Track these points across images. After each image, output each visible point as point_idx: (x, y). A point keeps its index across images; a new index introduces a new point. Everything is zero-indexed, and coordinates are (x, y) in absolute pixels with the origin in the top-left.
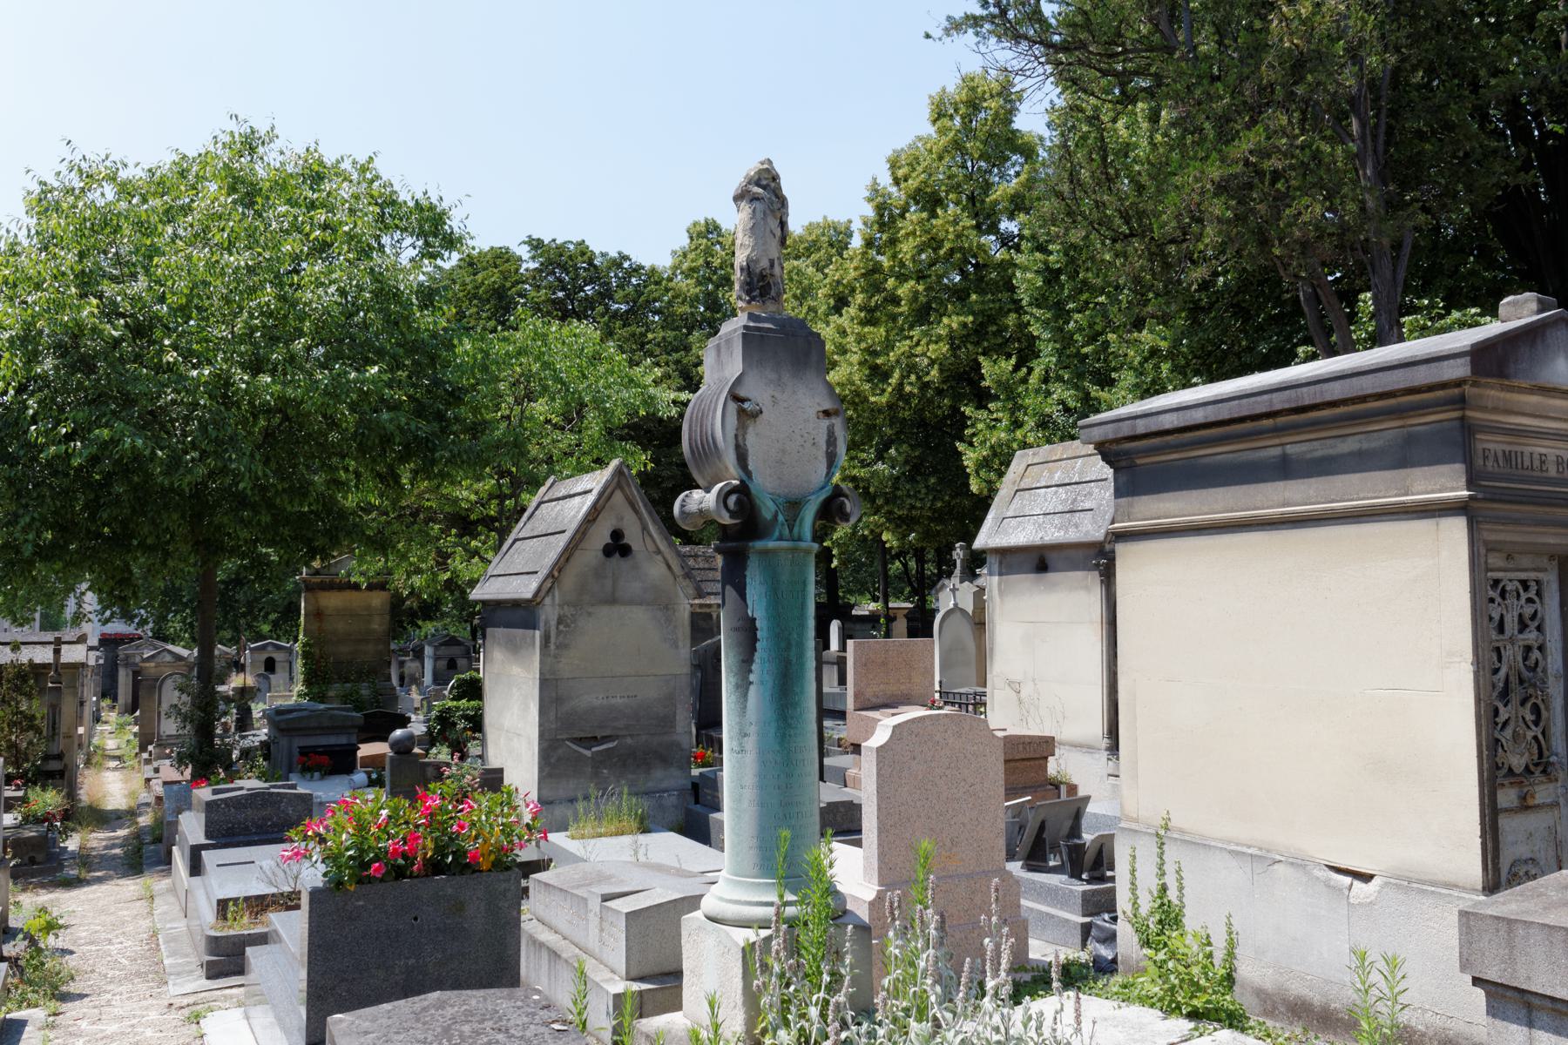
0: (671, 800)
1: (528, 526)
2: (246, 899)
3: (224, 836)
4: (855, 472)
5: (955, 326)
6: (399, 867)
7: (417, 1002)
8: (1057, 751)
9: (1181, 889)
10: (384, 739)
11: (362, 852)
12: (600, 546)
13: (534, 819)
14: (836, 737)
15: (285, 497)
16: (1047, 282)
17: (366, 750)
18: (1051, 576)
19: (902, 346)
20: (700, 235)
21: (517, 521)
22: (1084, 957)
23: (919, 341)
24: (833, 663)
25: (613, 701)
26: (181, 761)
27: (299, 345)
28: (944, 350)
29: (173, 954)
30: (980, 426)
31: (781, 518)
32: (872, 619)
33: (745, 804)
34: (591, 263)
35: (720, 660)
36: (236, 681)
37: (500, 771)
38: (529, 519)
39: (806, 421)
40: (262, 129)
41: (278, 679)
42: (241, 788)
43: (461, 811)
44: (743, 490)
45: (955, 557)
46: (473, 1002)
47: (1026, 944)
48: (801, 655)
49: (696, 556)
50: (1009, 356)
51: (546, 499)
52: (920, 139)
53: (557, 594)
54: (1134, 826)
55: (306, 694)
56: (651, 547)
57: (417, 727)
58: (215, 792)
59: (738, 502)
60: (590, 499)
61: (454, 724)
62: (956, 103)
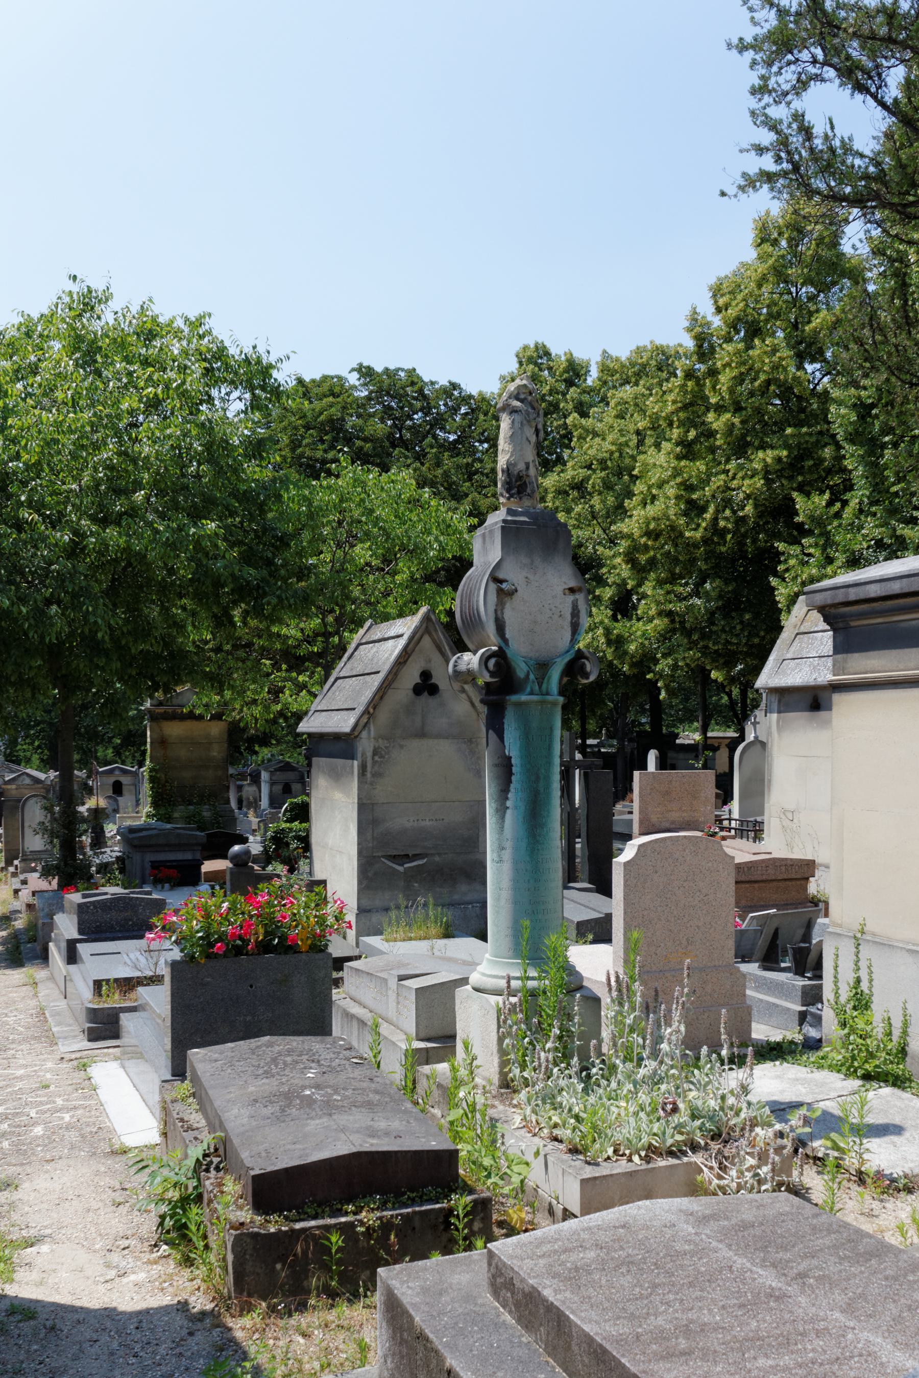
1: (348, 666)
2: (116, 980)
3: (93, 933)
4: (671, 606)
5: (769, 460)
6: (237, 946)
7: (253, 1043)
9: (871, 981)
10: (224, 856)
11: (206, 937)
12: (411, 685)
15: (131, 639)
16: (862, 417)
17: (209, 866)
19: (718, 481)
20: (531, 360)
21: (340, 658)
22: (799, 1038)
23: (735, 474)
25: (423, 824)
26: (46, 873)
27: (139, 496)
28: (759, 485)
29: (59, 1024)
30: (792, 562)
31: (532, 677)
32: (692, 749)
33: (503, 902)
34: (421, 391)
36: (91, 803)
38: (349, 658)
39: (554, 597)
40: (98, 285)
41: (125, 801)
42: (106, 894)
43: (284, 905)
44: (500, 655)
46: (295, 1044)
47: (750, 1026)
48: (548, 787)
50: (822, 492)
51: (364, 641)
52: (743, 264)
53: (372, 729)
54: (838, 930)
55: (154, 815)
57: (255, 846)
58: (84, 896)
59: (497, 664)
60: (402, 643)
61: (288, 844)
62: (779, 227)
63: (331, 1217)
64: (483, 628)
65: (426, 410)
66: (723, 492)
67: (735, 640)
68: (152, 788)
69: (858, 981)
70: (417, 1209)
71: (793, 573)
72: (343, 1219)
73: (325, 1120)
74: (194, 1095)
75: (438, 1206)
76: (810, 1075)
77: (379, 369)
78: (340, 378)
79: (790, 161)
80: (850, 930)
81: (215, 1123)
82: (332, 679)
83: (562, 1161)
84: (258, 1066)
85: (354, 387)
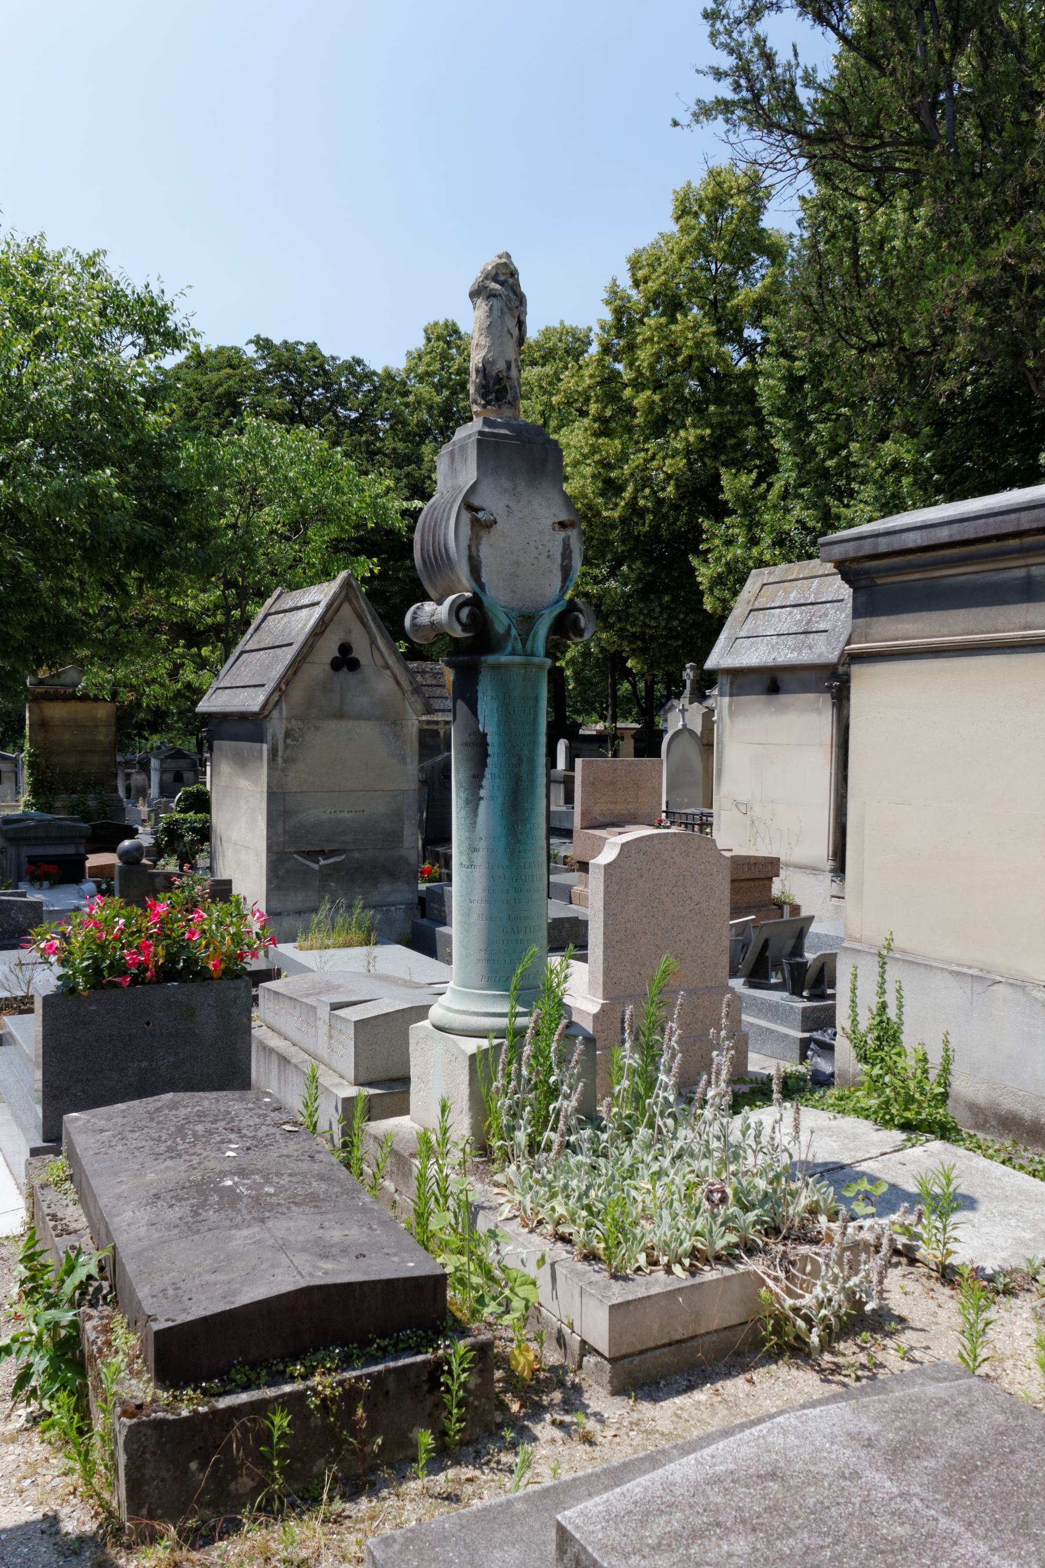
0: (398, 914)
1: (255, 638)
5: (691, 439)
8: (782, 872)
9: (900, 1007)
10: (113, 850)
13: (263, 928)
14: (562, 854)
17: (94, 860)
18: (783, 698)
21: (243, 633)
24: (560, 782)
25: (341, 815)
28: (681, 465)
31: (514, 632)
33: (474, 918)
34: (321, 367)
35: (449, 777)
37: (229, 882)
39: (542, 532)
44: (476, 603)
45: (685, 677)
46: (206, 1103)
47: (746, 1058)
48: (532, 771)
49: (423, 672)
50: (750, 472)
53: (284, 707)
55: (33, 805)
56: (380, 662)
57: (145, 838)
59: (471, 615)
60: (318, 611)
61: (182, 836)
63: (269, 1385)
64: (452, 569)
65: (327, 387)
66: (643, 470)
67: (653, 623)
68: (31, 775)
69: (884, 1006)
70: (392, 1364)
71: (716, 554)
72: (287, 1388)
73: (255, 1229)
74: (71, 1178)
75: (420, 1358)
76: (833, 1123)
77: (277, 341)
78: (237, 350)
79: (751, 89)
80: (872, 946)
81: (101, 1232)
82: (236, 652)
83: (579, 1274)
84: (159, 1140)
85: (253, 361)
